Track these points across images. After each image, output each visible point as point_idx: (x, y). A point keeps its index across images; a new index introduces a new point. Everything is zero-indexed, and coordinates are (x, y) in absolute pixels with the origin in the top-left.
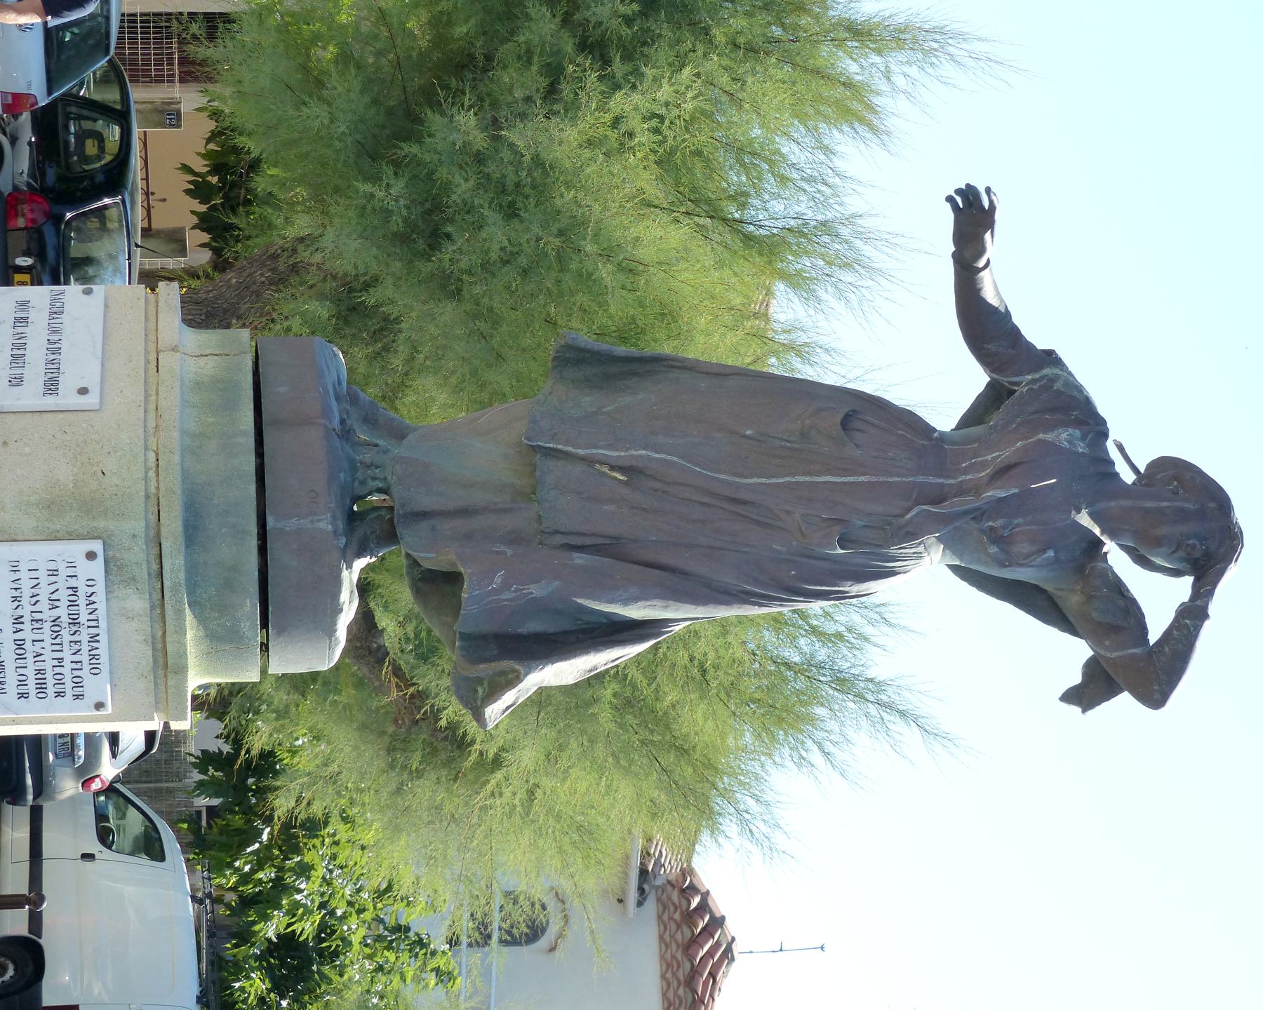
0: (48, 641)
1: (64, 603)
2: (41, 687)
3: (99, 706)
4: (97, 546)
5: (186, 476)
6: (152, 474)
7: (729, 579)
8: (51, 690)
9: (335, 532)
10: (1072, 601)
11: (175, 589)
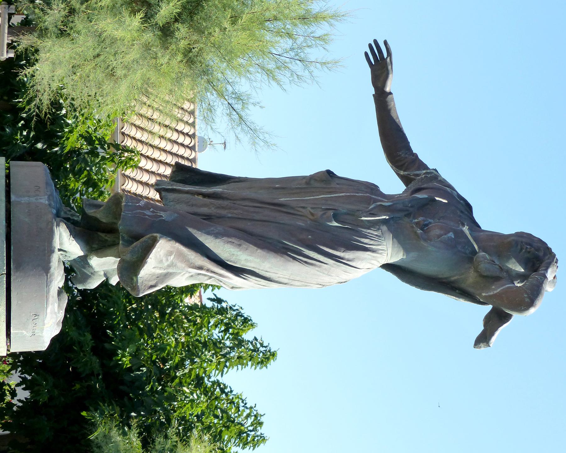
7: (272, 234)
9: (50, 205)
10: (470, 278)
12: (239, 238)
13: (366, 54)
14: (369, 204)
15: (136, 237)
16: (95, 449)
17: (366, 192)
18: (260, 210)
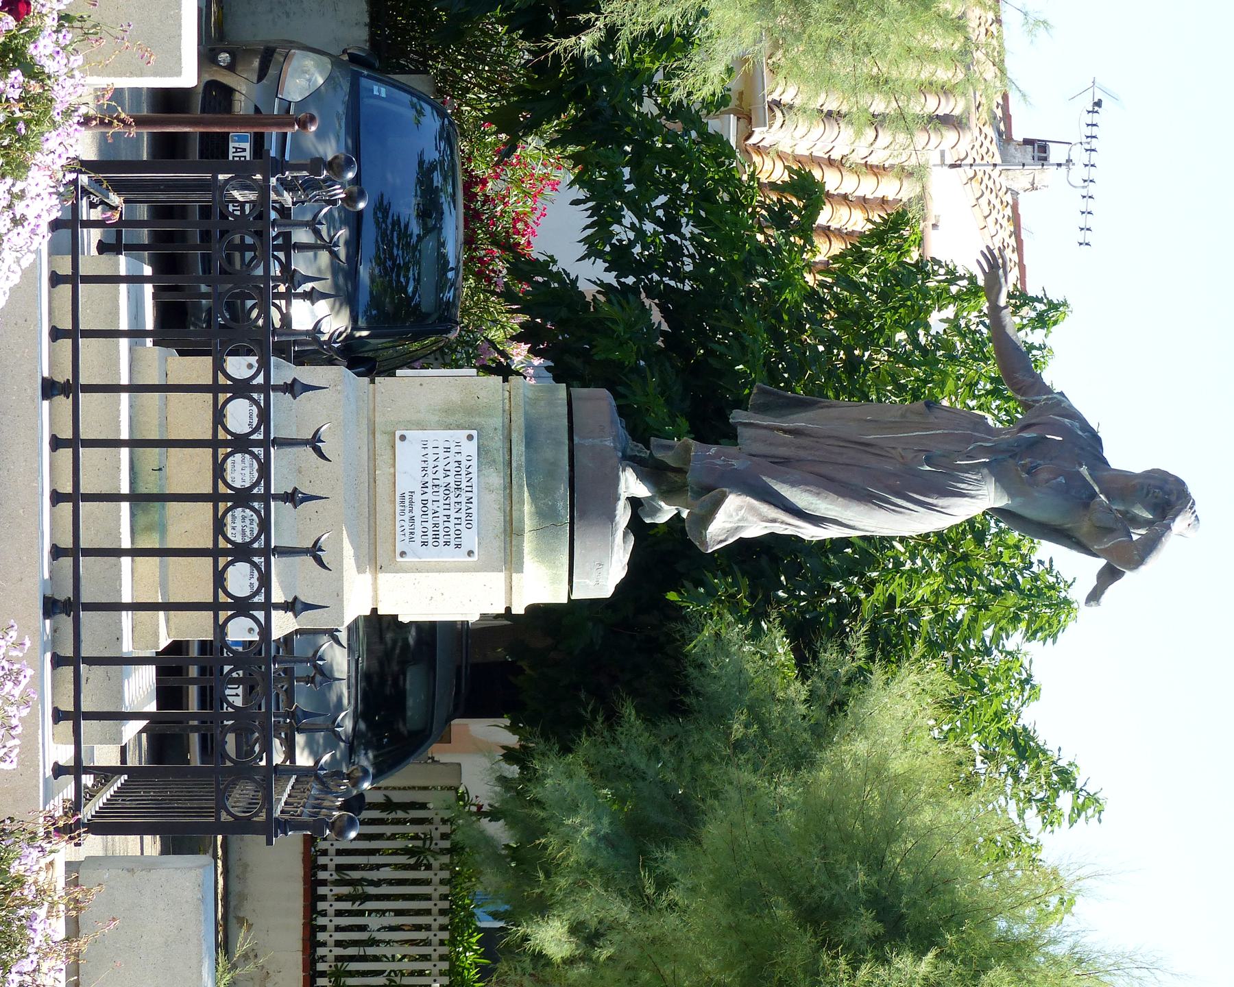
0: (442, 502)
1: (452, 473)
2: (436, 537)
3: (470, 553)
4: (474, 433)
5: (526, 413)
6: (507, 401)
8: (441, 541)
9: (615, 448)
10: (1084, 528)
11: (518, 469)
12: (817, 486)
13: (978, 262)
14: (969, 444)
15: (709, 489)
16: (691, 670)
17: (968, 429)
18: (844, 450)
